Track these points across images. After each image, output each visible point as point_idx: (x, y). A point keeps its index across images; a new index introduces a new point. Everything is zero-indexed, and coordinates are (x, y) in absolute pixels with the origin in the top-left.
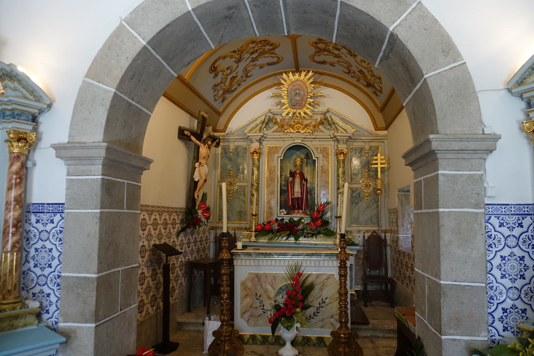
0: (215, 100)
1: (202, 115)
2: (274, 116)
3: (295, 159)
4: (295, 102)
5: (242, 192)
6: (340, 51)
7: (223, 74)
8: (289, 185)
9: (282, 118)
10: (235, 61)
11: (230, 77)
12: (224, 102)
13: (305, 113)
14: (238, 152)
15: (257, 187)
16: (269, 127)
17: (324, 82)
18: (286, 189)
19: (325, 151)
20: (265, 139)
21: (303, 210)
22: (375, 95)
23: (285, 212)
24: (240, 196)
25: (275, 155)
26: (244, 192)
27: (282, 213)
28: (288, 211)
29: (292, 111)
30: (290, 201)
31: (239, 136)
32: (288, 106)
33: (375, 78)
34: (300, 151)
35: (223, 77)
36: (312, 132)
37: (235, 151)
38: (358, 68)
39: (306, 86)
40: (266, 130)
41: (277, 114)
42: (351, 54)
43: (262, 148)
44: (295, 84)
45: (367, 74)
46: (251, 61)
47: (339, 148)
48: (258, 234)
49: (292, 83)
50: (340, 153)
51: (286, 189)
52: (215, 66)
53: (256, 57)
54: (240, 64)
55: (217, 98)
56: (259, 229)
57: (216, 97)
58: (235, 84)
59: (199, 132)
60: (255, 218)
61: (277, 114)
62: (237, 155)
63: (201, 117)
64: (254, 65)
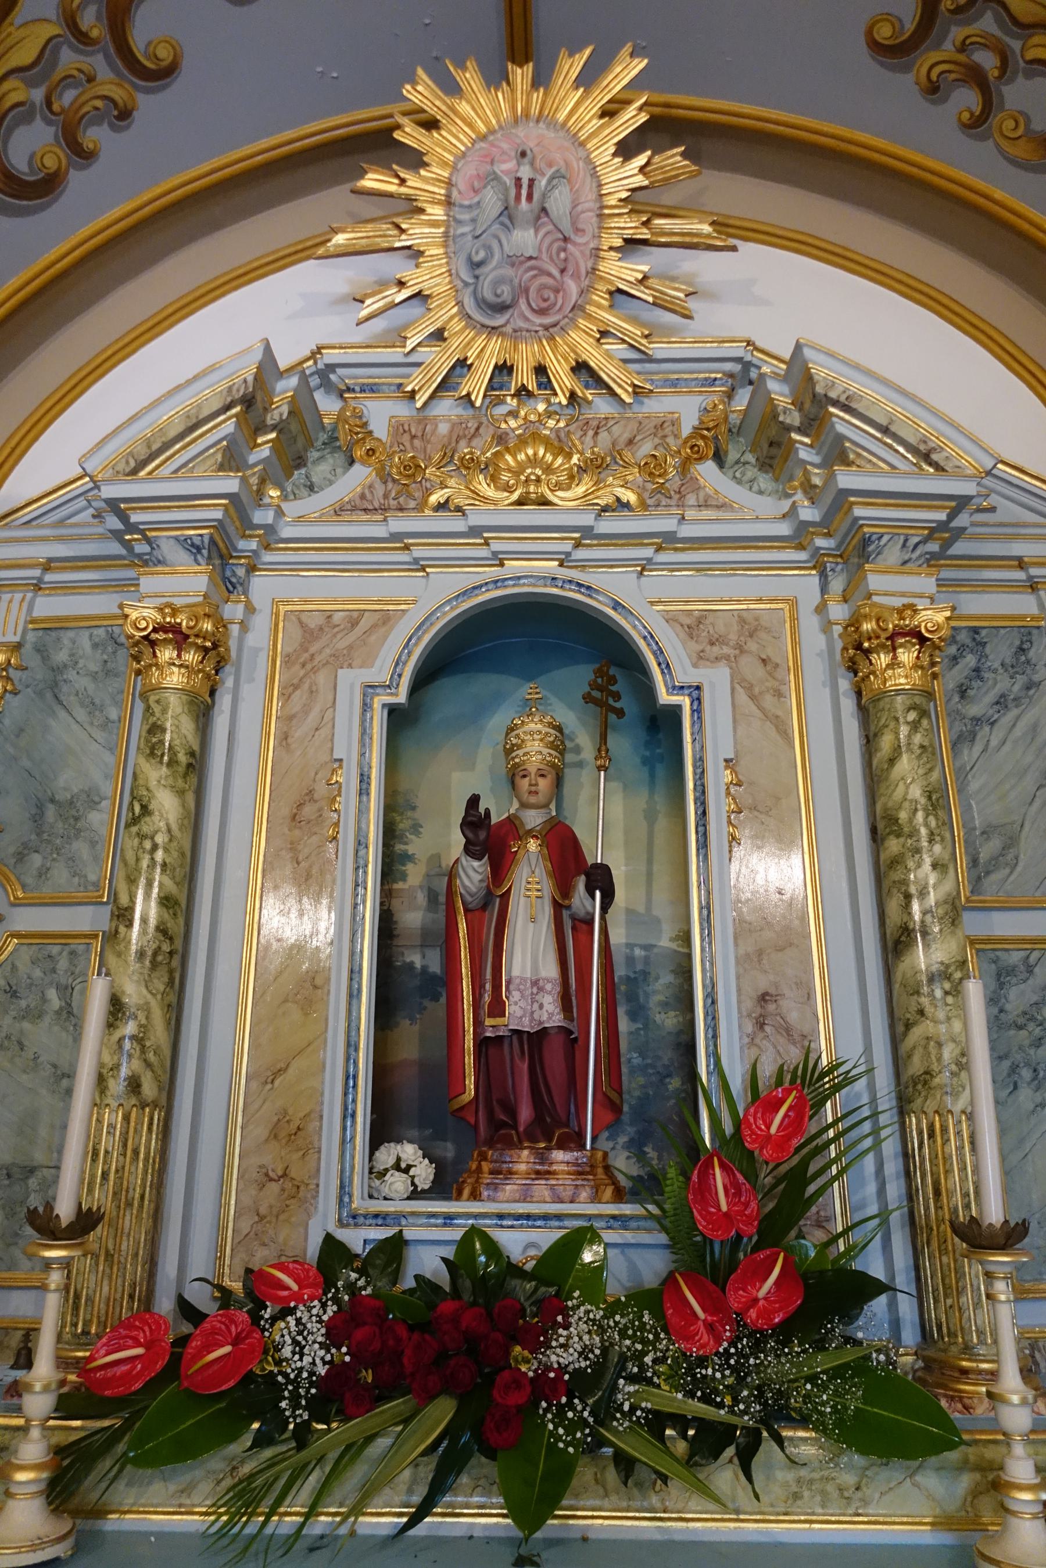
2: (342, 410)
3: (511, 729)
4: (509, 272)
5: (52, 994)
8: (462, 926)
9: (402, 410)
13: (581, 368)
14: (58, 670)
15: (162, 930)
18: (435, 966)
19: (752, 646)
20: (268, 557)
21: (582, 1146)
23: (424, 1173)
24: (26, 1025)
25: (340, 671)
26: (66, 991)
27: (397, 1183)
28: (448, 1150)
30: (469, 1060)
31: (60, 539)
32: (452, 318)
34: (543, 678)
36: (644, 505)
37: (33, 661)
39: (588, 161)
41: (372, 389)
43: (244, 626)
44: (505, 146)
47: (875, 598)
48: (113, 1437)
49: (483, 138)
50: (891, 638)
51: (435, 966)
56: (127, 1378)
60: (66, 1264)
61: (372, 389)
62: (40, 694)
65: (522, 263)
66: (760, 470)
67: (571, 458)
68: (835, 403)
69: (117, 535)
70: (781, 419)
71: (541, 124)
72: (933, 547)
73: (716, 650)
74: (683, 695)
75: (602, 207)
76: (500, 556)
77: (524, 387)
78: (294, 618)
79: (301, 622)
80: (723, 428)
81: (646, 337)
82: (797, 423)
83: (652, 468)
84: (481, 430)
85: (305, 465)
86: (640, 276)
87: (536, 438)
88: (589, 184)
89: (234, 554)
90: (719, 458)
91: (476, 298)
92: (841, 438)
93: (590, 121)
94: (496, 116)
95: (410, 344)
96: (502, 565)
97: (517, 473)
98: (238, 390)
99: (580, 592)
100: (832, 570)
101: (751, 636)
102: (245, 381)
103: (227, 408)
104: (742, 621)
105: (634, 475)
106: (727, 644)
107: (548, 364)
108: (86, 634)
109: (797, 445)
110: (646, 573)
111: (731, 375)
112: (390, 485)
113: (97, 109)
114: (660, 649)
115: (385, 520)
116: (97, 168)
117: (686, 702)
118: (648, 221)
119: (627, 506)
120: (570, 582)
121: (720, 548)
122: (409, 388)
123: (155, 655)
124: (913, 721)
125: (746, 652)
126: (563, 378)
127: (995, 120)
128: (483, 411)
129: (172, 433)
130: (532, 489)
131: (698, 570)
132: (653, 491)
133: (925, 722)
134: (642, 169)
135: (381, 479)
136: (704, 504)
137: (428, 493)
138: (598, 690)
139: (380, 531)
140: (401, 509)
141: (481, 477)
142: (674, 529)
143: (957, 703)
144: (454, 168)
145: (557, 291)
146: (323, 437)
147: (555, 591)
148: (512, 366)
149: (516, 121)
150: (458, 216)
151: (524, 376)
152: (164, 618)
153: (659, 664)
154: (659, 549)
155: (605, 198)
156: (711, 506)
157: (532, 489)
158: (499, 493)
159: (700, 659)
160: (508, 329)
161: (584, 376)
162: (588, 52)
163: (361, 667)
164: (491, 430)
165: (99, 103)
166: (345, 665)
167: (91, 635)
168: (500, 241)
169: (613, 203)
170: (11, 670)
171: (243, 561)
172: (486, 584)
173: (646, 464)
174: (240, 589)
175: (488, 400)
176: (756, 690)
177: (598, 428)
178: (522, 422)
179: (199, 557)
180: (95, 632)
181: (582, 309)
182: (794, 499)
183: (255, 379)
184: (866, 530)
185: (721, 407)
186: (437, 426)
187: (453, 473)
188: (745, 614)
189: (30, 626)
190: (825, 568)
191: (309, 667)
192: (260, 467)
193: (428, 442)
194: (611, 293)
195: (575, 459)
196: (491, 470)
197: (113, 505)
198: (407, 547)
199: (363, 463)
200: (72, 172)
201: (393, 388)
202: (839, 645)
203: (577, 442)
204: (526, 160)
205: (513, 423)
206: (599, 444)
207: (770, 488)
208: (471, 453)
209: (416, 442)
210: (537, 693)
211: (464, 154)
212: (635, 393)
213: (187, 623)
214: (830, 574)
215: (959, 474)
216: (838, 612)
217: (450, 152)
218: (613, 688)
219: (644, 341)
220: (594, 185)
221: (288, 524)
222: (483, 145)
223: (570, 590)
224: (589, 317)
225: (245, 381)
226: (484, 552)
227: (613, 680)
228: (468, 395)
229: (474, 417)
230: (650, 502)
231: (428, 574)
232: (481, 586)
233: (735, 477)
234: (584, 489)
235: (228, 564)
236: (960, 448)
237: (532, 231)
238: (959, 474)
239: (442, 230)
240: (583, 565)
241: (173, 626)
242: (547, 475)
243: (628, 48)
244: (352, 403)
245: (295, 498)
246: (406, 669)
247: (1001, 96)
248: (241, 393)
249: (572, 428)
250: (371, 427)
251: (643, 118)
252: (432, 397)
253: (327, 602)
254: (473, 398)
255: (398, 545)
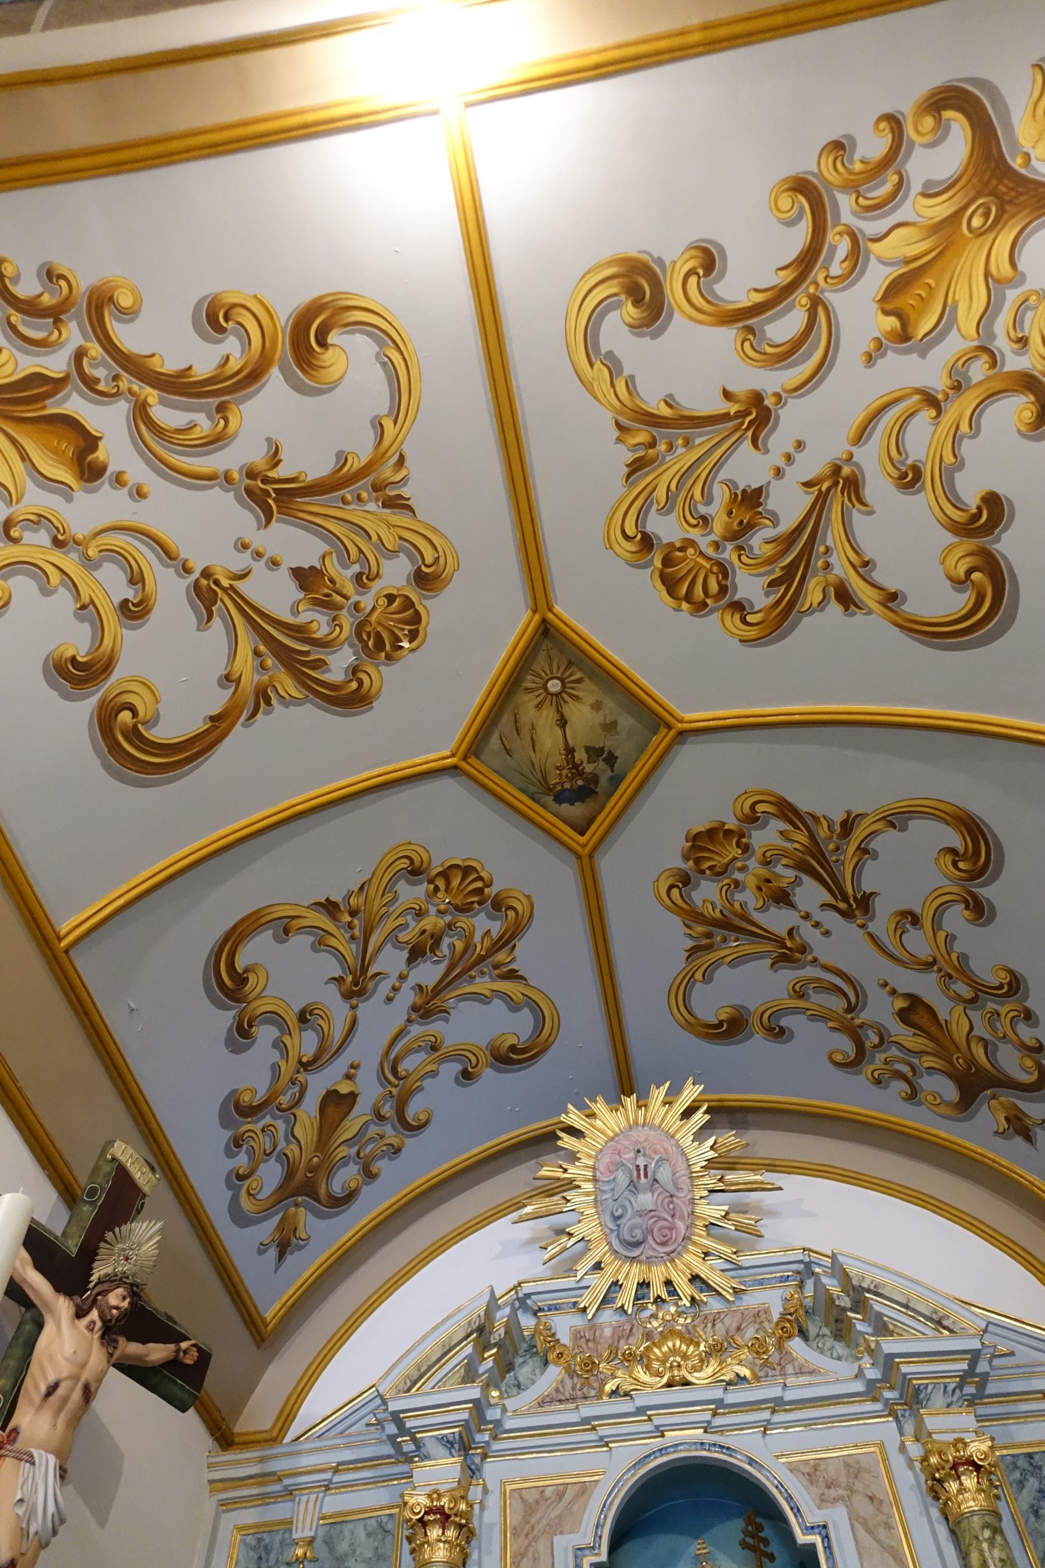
0: (240, 1218)
1: (114, 1159)
2: (537, 1325)
4: (638, 1221)
6: (791, 905)
7: (279, 1045)
10: (339, 980)
11: (318, 1084)
12: (290, 1259)
13: (695, 1278)
16: (519, 1386)
17: (759, 1155)
19: (859, 1486)
20: (496, 1446)
22: (1019, 1140)
25: (556, 1538)
29: (631, 1276)
31: (348, 1446)
32: (605, 1254)
33: (991, 1006)
35: (283, 1064)
36: (757, 1378)
38: (893, 992)
39: (678, 1145)
40: (501, 1397)
41: (556, 1308)
42: (842, 905)
44: (626, 1143)
45: (942, 1007)
46: (415, 1008)
49: (612, 1139)
50: (955, 1467)
52: (240, 965)
53: (439, 989)
54: (369, 1009)
55: (245, 1203)
57: (243, 1192)
58: (343, 1151)
59: (72, 1246)
61: (556, 1308)
63: (107, 1168)
64: (434, 1048)
65: (646, 1214)
66: (835, 1340)
67: (699, 1346)
68: (869, 1291)
69: (392, 1438)
70: (837, 1303)
71: (646, 1128)
72: (970, 1389)
73: (832, 1493)
74: (815, 1534)
75: (692, 1173)
76: (661, 1429)
77: (659, 1297)
78: (517, 1495)
79: (522, 1498)
80: (801, 1312)
81: (735, 1253)
82: (849, 1305)
83: (758, 1348)
84: (634, 1330)
85: (514, 1369)
86: (723, 1213)
87: (672, 1333)
88: (681, 1160)
89: (473, 1446)
90: (803, 1334)
91: (619, 1239)
92: (880, 1315)
93: (675, 1122)
94: (618, 1126)
95: (580, 1275)
96: (663, 1436)
97: (663, 1362)
98: (475, 1323)
99: (723, 1453)
100: (903, 1416)
101: (856, 1477)
102: (479, 1316)
103: (468, 1336)
104: (847, 1466)
105: (745, 1354)
106: (840, 1486)
107: (673, 1279)
108: (361, 1525)
109: (854, 1321)
110: (768, 1432)
111: (799, 1273)
112: (576, 1379)
113: (382, 1151)
114: (790, 1495)
115: (577, 1408)
116: (378, 1182)
117: (817, 1539)
118: (722, 1177)
119: (744, 1379)
120: (714, 1445)
121: (817, 1406)
122: (582, 1306)
123: (426, 1534)
124: (989, 1538)
125: (856, 1491)
126: (685, 1289)
127: (921, 1096)
128: (634, 1316)
129: (434, 1358)
130: (676, 1373)
131: (805, 1426)
132: (761, 1365)
133: (998, 1538)
134: (712, 1148)
135: (569, 1375)
136: (800, 1373)
137: (603, 1383)
138: (750, 1536)
139: (574, 1417)
140: (586, 1398)
141: (639, 1367)
142: (781, 1395)
143: (1034, 1522)
144: (596, 1158)
145: (671, 1229)
146: (524, 1346)
147: (704, 1453)
148: (649, 1282)
149: (630, 1127)
150: (602, 1188)
151: (658, 1289)
152: (432, 1502)
153: (792, 1509)
154: (774, 1411)
155: (692, 1167)
156: (804, 1373)
157: (676, 1373)
158: (653, 1378)
159: (822, 1501)
160: (643, 1257)
161: (698, 1284)
162: (668, 1084)
163: (570, 1533)
164: (641, 1330)
165: (384, 1148)
166: (558, 1533)
167: (365, 1526)
168: (630, 1202)
169: (698, 1169)
170: (306, 1562)
171: (479, 1451)
172: (654, 1452)
173: (752, 1345)
174: (478, 1474)
175: (636, 1308)
176: (871, 1524)
177: (714, 1320)
178: (661, 1322)
179: (453, 1450)
180: (369, 1522)
181: (690, 1239)
182: (861, 1362)
183: (485, 1314)
184: (914, 1382)
185: (796, 1296)
186: (603, 1330)
187: (618, 1366)
188: (848, 1460)
189: (321, 1522)
190: (897, 1414)
191: (531, 1536)
192: (486, 1375)
193: (599, 1343)
194: (706, 1226)
195: (702, 1347)
196: (644, 1360)
197: (396, 1418)
198: (594, 1428)
199: (555, 1364)
200: (364, 1187)
201: (570, 1305)
202: (922, 1478)
203: (701, 1333)
204: (640, 1154)
205: (655, 1324)
206: (717, 1333)
207: (846, 1353)
208: (629, 1349)
209: (591, 1344)
210: (704, 1548)
211: (601, 1150)
212: (735, 1292)
213: (449, 1504)
214: (901, 1419)
215: (963, 1333)
216: (915, 1450)
217: (593, 1150)
218: (762, 1535)
219: (734, 1256)
220: (684, 1160)
221: (510, 1418)
222: (612, 1143)
223: (716, 1452)
224: (695, 1243)
225: (479, 1316)
226: (648, 1427)
227: (760, 1528)
228: (623, 1306)
229: (628, 1321)
230: (761, 1374)
231: (610, 1448)
232: (650, 1455)
233: (818, 1347)
234: (712, 1369)
235: (468, 1454)
236: (960, 1315)
237: (650, 1194)
238: (963, 1333)
239: (593, 1197)
240: (721, 1430)
241: (438, 1509)
242: (685, 1361)
243: (690, 1080)
244: (543, 1319)
245: (509, 1397)
246: (605, 1530)
247: (919, 1084)
248: (477, 1325)
249: (696, 1322)
250: (558, 1336)
251: (707, 1117)
252: (598, 1309)
253: (539, 1479)
254: (626, 1308)
255: (587, 1427)
